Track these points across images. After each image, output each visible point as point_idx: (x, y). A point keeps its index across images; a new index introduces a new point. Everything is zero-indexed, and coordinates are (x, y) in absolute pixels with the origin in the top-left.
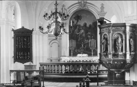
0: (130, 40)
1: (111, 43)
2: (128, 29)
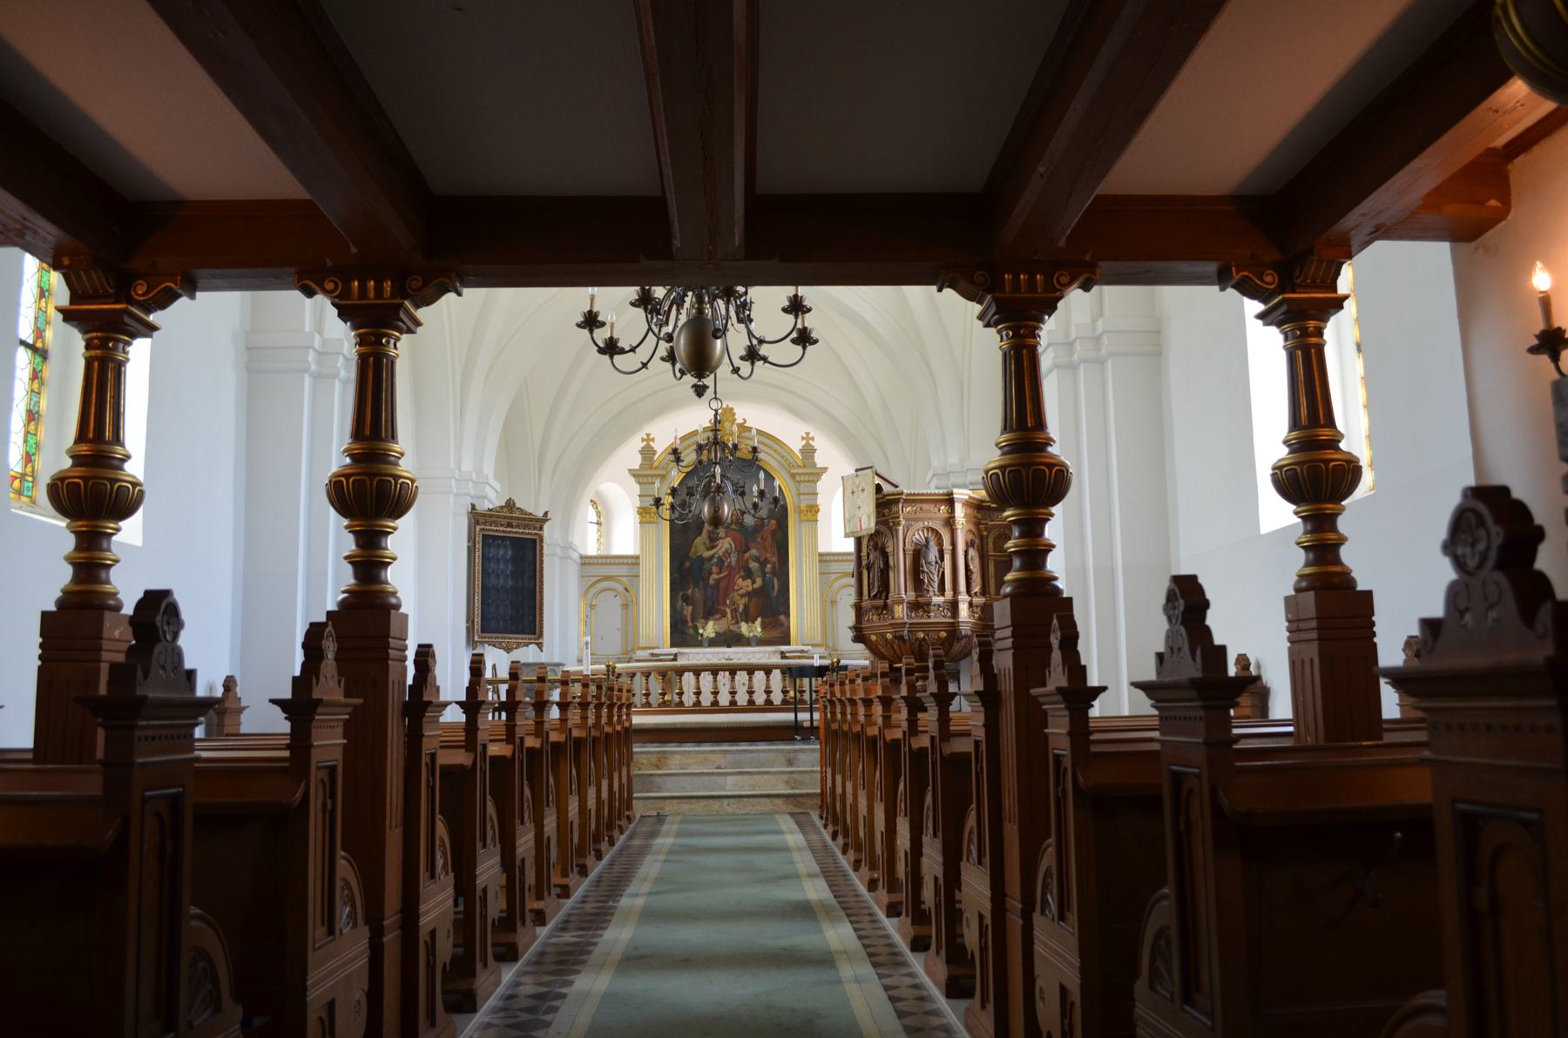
0: (966, 553)
1: (901, 563)
2: (960, 512)
